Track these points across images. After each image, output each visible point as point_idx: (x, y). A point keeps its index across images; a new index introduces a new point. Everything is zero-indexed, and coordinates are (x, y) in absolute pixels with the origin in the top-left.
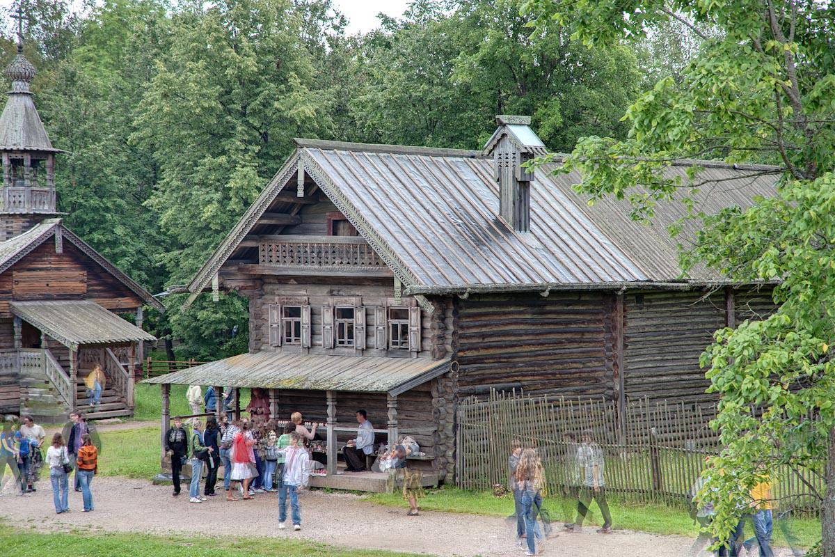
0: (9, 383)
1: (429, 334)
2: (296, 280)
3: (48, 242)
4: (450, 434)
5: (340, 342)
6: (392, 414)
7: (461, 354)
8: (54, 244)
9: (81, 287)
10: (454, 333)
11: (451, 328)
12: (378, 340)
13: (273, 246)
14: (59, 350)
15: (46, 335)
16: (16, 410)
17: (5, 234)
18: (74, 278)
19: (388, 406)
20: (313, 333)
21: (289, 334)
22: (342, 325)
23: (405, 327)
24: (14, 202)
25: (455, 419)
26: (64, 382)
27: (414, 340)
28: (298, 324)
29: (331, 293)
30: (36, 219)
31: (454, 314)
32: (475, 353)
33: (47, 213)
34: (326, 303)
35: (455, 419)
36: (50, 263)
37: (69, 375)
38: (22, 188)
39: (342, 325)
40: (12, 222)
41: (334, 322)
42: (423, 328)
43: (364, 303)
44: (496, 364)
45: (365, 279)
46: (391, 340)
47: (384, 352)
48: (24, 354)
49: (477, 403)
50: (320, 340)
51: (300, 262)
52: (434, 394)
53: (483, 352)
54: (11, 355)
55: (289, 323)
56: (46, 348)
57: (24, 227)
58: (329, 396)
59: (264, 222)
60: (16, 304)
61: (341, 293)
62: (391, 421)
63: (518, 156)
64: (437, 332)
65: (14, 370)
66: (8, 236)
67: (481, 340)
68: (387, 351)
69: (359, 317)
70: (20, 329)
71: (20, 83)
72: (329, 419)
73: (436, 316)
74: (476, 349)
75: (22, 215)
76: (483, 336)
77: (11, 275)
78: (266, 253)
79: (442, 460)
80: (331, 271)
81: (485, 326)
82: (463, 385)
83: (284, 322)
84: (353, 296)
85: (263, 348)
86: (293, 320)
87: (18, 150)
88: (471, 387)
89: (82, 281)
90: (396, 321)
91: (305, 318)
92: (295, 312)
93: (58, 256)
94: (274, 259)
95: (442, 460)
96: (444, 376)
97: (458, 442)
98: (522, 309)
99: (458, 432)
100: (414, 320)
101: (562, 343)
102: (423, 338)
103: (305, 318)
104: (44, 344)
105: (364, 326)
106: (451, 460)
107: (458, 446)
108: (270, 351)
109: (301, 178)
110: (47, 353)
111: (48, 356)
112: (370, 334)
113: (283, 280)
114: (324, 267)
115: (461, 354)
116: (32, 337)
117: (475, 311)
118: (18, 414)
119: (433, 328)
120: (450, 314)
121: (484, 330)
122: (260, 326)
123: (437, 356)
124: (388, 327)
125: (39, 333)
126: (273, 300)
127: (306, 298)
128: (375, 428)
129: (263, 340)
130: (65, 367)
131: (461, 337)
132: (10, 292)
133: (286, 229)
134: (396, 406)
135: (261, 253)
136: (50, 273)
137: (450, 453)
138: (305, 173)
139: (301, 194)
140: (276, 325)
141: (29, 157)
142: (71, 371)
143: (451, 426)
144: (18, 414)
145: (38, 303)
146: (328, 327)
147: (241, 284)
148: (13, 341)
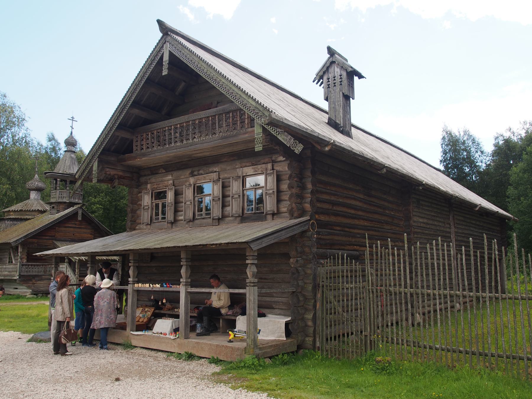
2: (164, 169)
3: (74, 215)
4: (309, 295)
6: (250, 271)
11: (309, 186)
17: (56, 211)
19: (248, 262)
20: (176, 211)
21: (157, 214)
24: (61, 197)
25: (315, 279)
29: (192, 175)
30: (71, 204)
31: (312, 173)
35: (315, 279)
36: (76, 225)
40: (60, 206)
41: (152, 203)
44: (342, 233)
45: (223, 155)
50: (181, 216)
52: (293, 253)
53: (333, 219)
57: (65, 208)
58: (183, 255)
66: (58, 212)
71: (70, 147)
73: (294, 175)
83: (154, 204)
84: (212, 172)
85: (137, 228)
88: (323, 251)
89: (91, 234)
94: (144, 147)
98: (358, 188)
99: (319, 295)
101: (382, 223)
105: (221, 197)
106: (310, 323)
108: (261, 370)
112: (227, 204)
120: (308, 173)
121: (333, 198)
123: (296, 214)
126: (146, 188)
127: (171, 182)
128: (229, 287)
129: (138, 221)
132: (54, 236)
134: (256, 262)
136: (75, 229)
137: (309, 316)
140: (147, 207)
143: (310, 288)
147: (121, 173)
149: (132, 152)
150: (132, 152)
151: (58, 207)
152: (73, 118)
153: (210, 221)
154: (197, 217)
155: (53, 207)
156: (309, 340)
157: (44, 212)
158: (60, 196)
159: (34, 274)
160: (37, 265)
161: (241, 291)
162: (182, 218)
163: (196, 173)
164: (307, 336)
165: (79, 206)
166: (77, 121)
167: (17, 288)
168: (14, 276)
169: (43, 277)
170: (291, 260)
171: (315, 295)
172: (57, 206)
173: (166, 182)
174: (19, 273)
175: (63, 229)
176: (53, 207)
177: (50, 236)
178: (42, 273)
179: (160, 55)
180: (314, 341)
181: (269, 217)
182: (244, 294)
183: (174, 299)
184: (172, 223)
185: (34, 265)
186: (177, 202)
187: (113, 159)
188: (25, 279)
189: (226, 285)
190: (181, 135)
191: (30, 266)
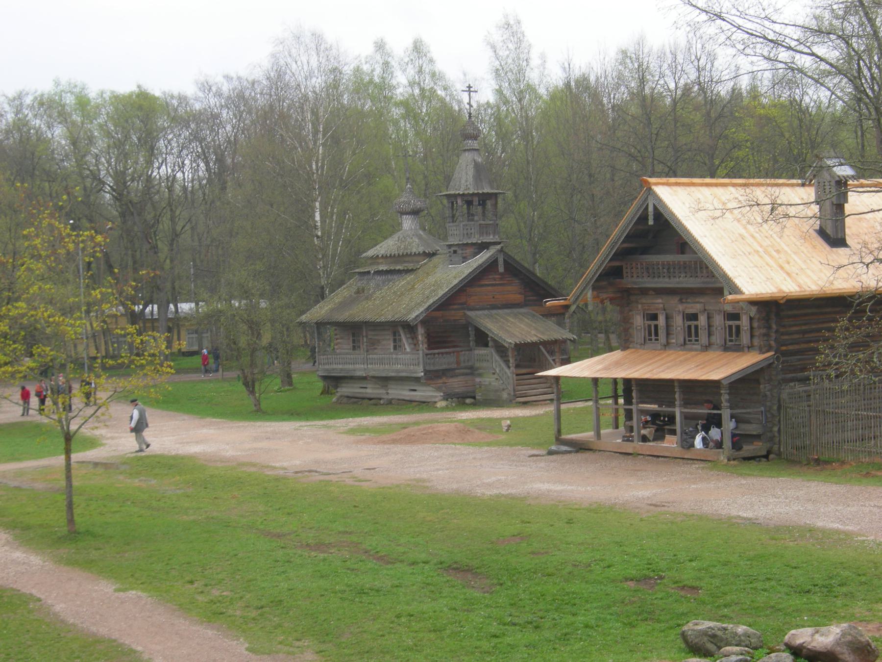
0: (467, 374)
1: (757, 333)
5: (690, 341)
7: (784, 348)
8: (498, 265)
9: (519, 298)
10: (777, 331)
11: (774, 326)
12: (717, 338)
13: (634, 264)
14: (501, 350)
15: (492, 337)
16: (472, 395)
18: (513, 291)
19: (722, 392)
21: (650, 334)
22: (689, 327)
23: (738, 328)
24: (467, 234)
25: (779, 401)
26: (506, 373)
27: (745, 338)
28: (656, 327)
29: (681, 301)
30: (483, 246)
32: (796, 347)
33: (492, 241)
34: (677, 309)
35: (779, 401)
36: (495, 280)
37: (509, 367)
38: (473, 223)
39: (689, 327)
41: (644, 324)
42: (752, 328)
43: (707, 308)
46: (728, 338)
47: (722, 348)
48: (476, 352)
49: (799, 388)
50: (673, 339)
51: (659, 277)
52: (762, 381)
54: (467, 352)
55: (650, 326)
56: (492, 347)
59: (625, 245)
60: (469, 313)
61: (689, 300)
62: (725, 404)
63: (833, 183)
64: (764, 331)
65: (470, 364)
67: (801, 336)
68: (726, 348)
69: (702, 320)
70: (474, 332)
72: (677, 403)
74: (797, 344)
75: (473, 244)
76: (804, 332)
77: (465, 291)
78: (629, 270)
79: (769, 434)
80: (678, 283)
81: (805, 324)
82: (786, 374)
84: (698, 302)
86: (653, 323)
87: (468, 193)
89: (520, 293)
90: (731, 323)
91: (661, 321)
92: (655, 317)
93: (501, 274)
95: (769, 434)
96: (770, 365)
97: (782, 419)
98: (838, 309)
100: (744, 322)
102: (752, 336)
103: (661, 321)
104: (490, 344)
105: (707, 327)
106: (776, 434)
107: (782, 423)
109: (651, 209)
110: (493, 351)
111: (494, 353)
113: (644, 292)
114: (672, 280)
115: (784, 348)
116: (482, 338)
117: (795, 312)
118: (474, 398)
119: (759, 328)
120: (773, 316)
121: (804, 328)
122: (629, 329)
124: (725, 328)
125: (487, 335)
126: (638, 308)
129: (631, 339)
130: (507, 362)
131: (783, 334)
132: (465, 303)
133: (645, 251)
135: (624, 271)
137: (776, 429)
138: (654, 205)
139: (651, 222)
141: (477, 199)
142: (511, 365)
143: (775, 408)
144: (474, 398)
145: (486, 312)
146: (679, 328)
148: (469, 342)
149: (623, 278)
150: (623, 278)
151: (464, 252)
152: (469, 87)
153: (699, 347)
154: (687, 342)
155: (455, 252)
156: (776, 448)
157: (433, 254)
158: (465, 232)
159: (444, 367)
160: (447, 353)
161: (719, 412)
162: (674, 341)
163: (684, 301)
164: (775, 444)
165: (499, 247)
166: (476, 92)
167: (415, 390)
168: (415, 373)
169: (457, 371)
170: (761, 386)
171: (780, 414)
172: (461, 252)
173: (657, 305)
174: (424, 367)
175: (478, 289)
176: (455, 252)
177: (459, 304)
178: (454, 366)
179: (645, 206)
180: (779, 448)
181: (746, 349)
182: (720, 415)
183: (672, 419)
184: (665, 346)
185: (442, 353)
186: (668, 326)
187: (604, 283)
188: (432, 376)
189: (762, 369)
190: (669, 272)
191: (437, 356)
